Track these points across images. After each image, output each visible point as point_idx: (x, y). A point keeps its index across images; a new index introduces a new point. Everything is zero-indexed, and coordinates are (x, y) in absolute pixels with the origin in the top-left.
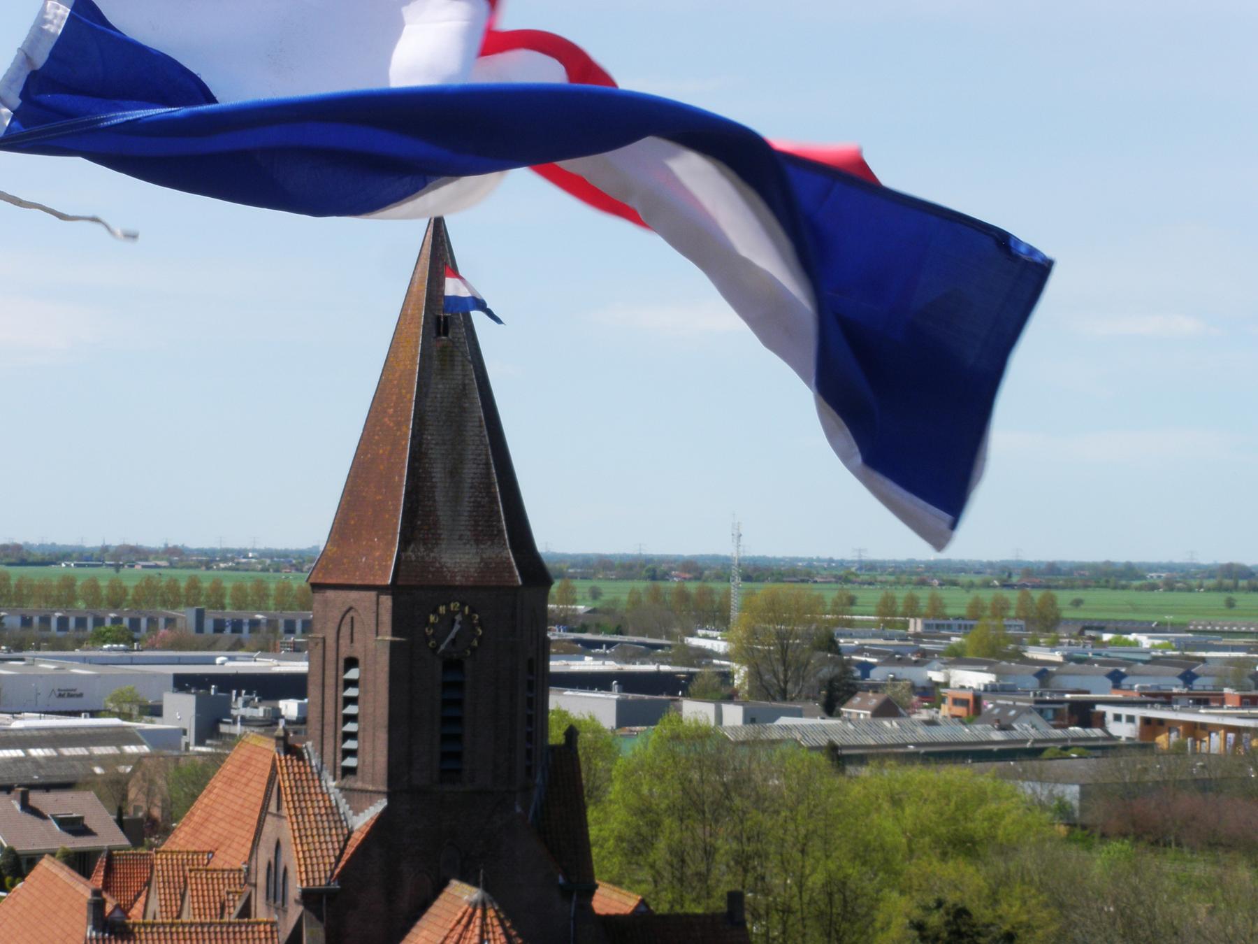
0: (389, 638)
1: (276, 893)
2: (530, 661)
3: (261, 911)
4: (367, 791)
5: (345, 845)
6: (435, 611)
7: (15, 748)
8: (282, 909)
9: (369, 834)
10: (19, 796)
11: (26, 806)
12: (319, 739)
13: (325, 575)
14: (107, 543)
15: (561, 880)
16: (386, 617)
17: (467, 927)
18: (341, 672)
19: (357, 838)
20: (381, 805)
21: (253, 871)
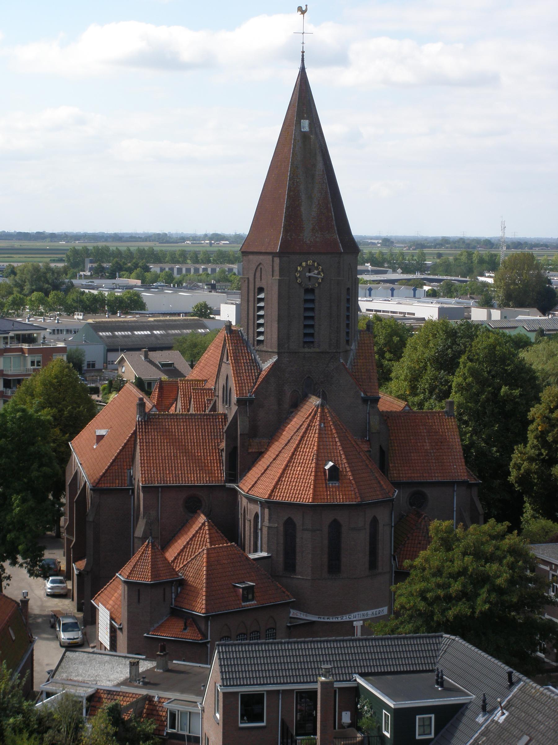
0: (278, 278)
1: (227, 400)
2: (348, 289)
3: (221, 409)
4: (268, 352)
5: (258, 377)
6: (300, 265)
7: (146, 330)
8: (230, 408)
9: (269, 372)
10: (143, 353)
11: (146, 356)
12: (246, 327)
13: (249, 248)
14: (207, 233)
15: (362, 395)
16: (277, 268)
17: (314, 417)
18: (256, 294)
19: (264, 373)
20: (275, 358)
21: (217, 390)
